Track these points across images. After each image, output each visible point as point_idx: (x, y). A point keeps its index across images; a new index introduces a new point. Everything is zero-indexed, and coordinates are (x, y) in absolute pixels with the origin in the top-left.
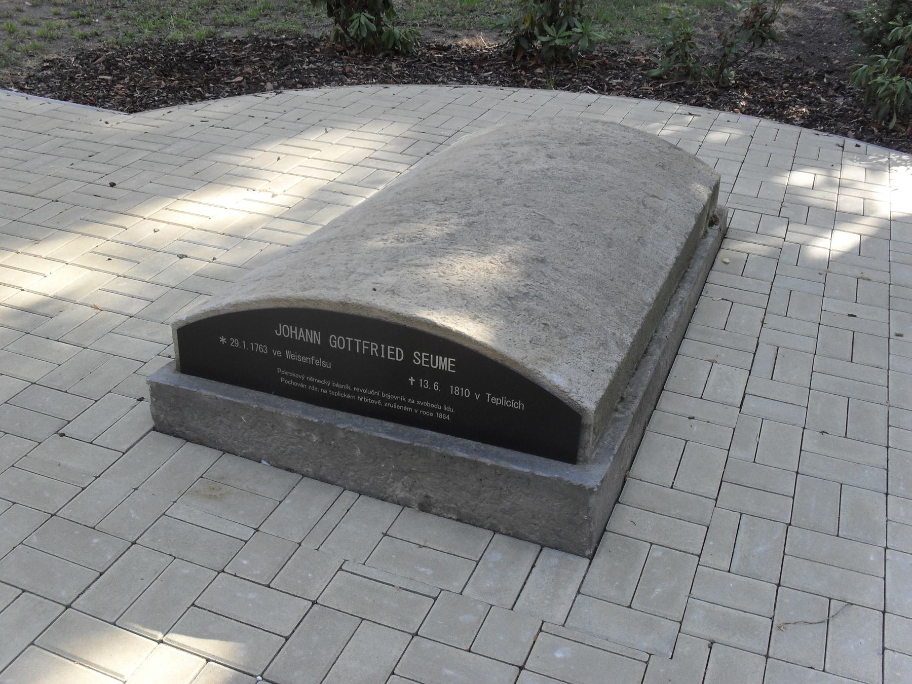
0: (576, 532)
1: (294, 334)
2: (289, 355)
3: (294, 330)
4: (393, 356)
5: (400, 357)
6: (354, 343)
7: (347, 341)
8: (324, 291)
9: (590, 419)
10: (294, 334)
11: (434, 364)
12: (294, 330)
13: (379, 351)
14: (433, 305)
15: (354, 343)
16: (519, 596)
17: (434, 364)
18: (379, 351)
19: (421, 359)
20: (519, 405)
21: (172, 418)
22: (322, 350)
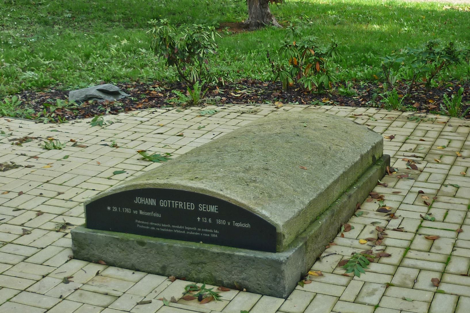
2: (141, 212)
7: (168, 202)
19: (202, 208)
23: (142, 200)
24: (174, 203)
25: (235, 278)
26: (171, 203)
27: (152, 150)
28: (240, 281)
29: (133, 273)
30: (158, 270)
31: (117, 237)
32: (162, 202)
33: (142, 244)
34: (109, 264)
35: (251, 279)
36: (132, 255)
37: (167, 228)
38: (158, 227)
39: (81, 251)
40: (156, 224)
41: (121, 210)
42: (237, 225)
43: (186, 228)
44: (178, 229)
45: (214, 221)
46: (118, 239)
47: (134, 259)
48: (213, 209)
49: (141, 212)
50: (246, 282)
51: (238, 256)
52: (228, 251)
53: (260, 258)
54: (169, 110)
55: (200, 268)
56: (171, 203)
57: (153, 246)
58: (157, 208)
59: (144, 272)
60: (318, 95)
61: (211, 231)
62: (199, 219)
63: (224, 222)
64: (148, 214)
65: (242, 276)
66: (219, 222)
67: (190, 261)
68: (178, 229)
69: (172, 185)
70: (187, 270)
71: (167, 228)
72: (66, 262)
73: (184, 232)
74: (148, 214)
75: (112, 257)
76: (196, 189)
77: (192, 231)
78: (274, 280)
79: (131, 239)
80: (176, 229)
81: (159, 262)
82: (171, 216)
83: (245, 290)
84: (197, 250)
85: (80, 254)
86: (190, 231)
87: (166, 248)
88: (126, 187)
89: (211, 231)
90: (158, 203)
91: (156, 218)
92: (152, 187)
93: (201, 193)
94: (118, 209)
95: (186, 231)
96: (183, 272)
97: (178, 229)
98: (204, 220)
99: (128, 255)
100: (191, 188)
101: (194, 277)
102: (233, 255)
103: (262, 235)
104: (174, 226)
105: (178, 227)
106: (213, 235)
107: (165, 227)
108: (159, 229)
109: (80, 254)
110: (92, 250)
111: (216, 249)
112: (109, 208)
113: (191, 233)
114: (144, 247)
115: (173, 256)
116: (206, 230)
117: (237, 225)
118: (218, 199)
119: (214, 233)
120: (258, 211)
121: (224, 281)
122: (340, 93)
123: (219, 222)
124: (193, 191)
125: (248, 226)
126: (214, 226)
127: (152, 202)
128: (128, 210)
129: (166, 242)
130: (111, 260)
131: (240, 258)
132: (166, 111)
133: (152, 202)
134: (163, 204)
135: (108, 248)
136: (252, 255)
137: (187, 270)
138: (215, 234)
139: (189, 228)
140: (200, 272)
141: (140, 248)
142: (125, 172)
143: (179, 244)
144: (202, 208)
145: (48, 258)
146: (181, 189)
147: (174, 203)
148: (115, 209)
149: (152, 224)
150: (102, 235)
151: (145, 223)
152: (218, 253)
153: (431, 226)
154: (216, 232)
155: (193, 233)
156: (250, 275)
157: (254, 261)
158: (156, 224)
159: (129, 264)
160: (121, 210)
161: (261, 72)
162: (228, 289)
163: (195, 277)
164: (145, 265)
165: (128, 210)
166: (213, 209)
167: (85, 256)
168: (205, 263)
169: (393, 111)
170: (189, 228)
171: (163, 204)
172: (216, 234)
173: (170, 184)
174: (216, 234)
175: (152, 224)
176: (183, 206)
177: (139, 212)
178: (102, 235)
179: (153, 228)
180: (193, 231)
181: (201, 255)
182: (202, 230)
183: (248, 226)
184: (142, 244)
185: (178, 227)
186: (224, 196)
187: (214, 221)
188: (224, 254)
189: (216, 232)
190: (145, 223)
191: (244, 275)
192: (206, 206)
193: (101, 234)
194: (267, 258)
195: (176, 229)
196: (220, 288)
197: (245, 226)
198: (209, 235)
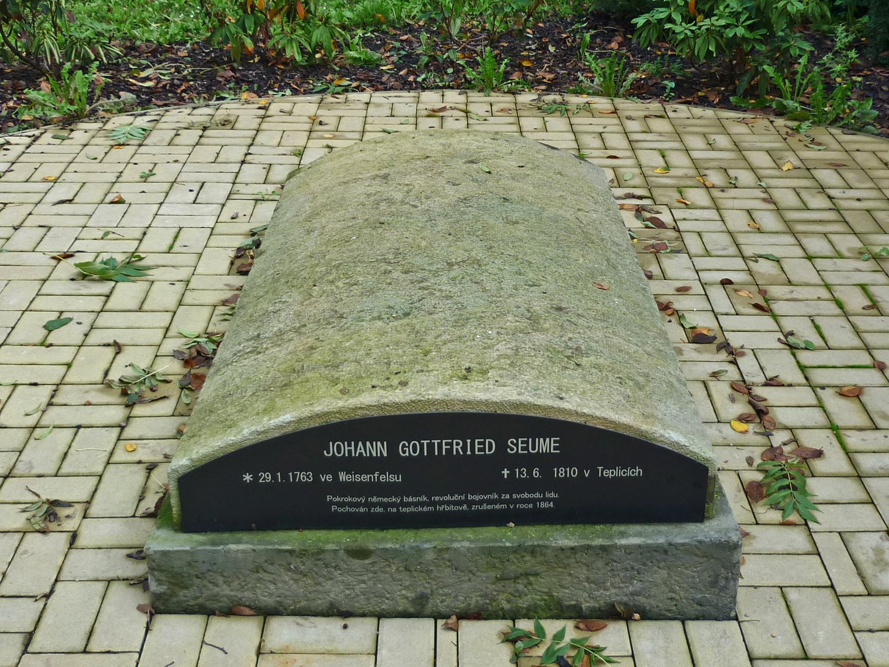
1: (350, 451)
2: (343, 477)
3: (349, 445)
5: (490, 450)
7: (422, 445)
12: (349, 445)
13: (464, 448)
19: (516, 446)
20: (393, 478)
23: (345, 448)
24: (440, 445)
25: (613, 593)
26: (431, 447)
27: (91, 250)
28: (625, 599)
29: (345, 627)
30: (402, 605)
31: (288, 547)
32: (404, 446)
33: (361, 553)
34: (266, 613)
35: (654, 591)
36: (330, 582)
37: (416, 504)
38: (393, 505)
39: (168, 592)
40: (385, 500)
41: (285, 476)
42: (609, 473)
43: (470, 497)
44: (448, 502)
45: (547, 472)
46: (291, 552)
47: (334, 591)
48: (546, 445)
49: (343, 477)
50: (641, 600)
51: (626, 547)
52: (596, 536)
53: (683, 545)
54: (36, 138)
55: (521, 587)
56: (431, 447)
57: (389, 555)
58: (391, 463)
59: (364, 615)
60: (312, 73)
61: (537, 495)
62: (506, 472)
63: (573, 472)
64: (365, 478)
65: (631, 589)
66: (561, 473)
67: (492, 574)
68: (448, 503)
69: (432, 402)
70: (485, 596)
71: (416, 504)
72: (148, 629)
73: (465, 507)
74: (365, 478)
75: (271, 595)
76: (501, 404)
77: (485, 501)
78: (714, 584)
79: (330, 547)
80: (441, 503)
81: (407, 588)
82: (422, 475)
83: (637, 616)
84: (518, 549)
85: (175, 599)
86: (480, 503)
87: (430, 556)
88: (300, 421)
89: (537, 495)
90: (392, 449)
91: (388, 484)
92: (375, 413)
93: (513, 412)
94: (274, 477)
95: (470, 503)
96: (475, 600)
97: (448, 503)
98: (520, 473)
99: (319, 584)
100: (486, 403)
101: (502, 609)
102: (615, 546)
103: (676, 486)
104: (437, 498)
105: (448, 498)
106: (544, 505)
107: (415, 503)
108: (395, 510)
109: (175, 599)
110: (211, 586)
111: (564, 537)
112: (248, 478)
113: (485, 507)
114: (367, 561)
115: (448, 571)
116: (526, 495)
117: (609, 473)
118: (659, 447)
119: (545, 499)
120: (662, 436)
121: (583, 606)
122: (350, 61)
123: (561, 473)
124: (491, 410)
125: (638, 471)
126: (547, 483)
127: (379, 449)
128: (303, 477)
129: (429, 540)
130: (268, 601)
131: (629, 550)
132: (29, 140)
133: (379, 449)
134: (407, 449)
135: (262, 575)
136: (661, 540)
137: (485, 596)
138: (547, 501)
139: (477, 498)
140: (521, 595)
141: (356, 563)
142: (71, 319)
143: (464, 540)
144: (516, 446)
145: (88, 629)
146: (457, 409)
147: (440, 445)
148: (266, 477)
149: (375, 499)
150: (242, 547)
151: (355, 499)
152: (572, 549)
153: (856, 364)
154: (552, 495)
155: (489, 507)
156: (656, 584)
157: (666, 552)
158: (385, 500)
159: (321, 603)
160: (285, 476)
161: (146, 25)
162: (601, 622)
163: (506, 606)
164: (368, 599)
165: (303, 477)
166: (546, 445)
167: (192, 603)
168: (536, 575)
169: (492, 94)
170: (477, 498)
171: (407, 449)
172: (549, 500)
173: (428, 401)
174: (549, 500)
175: (375, 499)
176: (464, 448)
177: (336, 477)
178: (242, 547)
179: (379, 510)
180: (490, 502)
181: (527, 558)
182: (514, 496)
183: (638, 471)
184: (361, 553)
185: (448, 498)
186: (569, 412)
187: (547, 472)
188: (589, 547)
189: (552, 495)
190: (355, 499)
191: (637, 585)
192: (527, 442)
193: (241, 545)
194: (700, 542)
195: (441, 503)
196: (581, 626)
197: (629, 473)
198: (531, 506)
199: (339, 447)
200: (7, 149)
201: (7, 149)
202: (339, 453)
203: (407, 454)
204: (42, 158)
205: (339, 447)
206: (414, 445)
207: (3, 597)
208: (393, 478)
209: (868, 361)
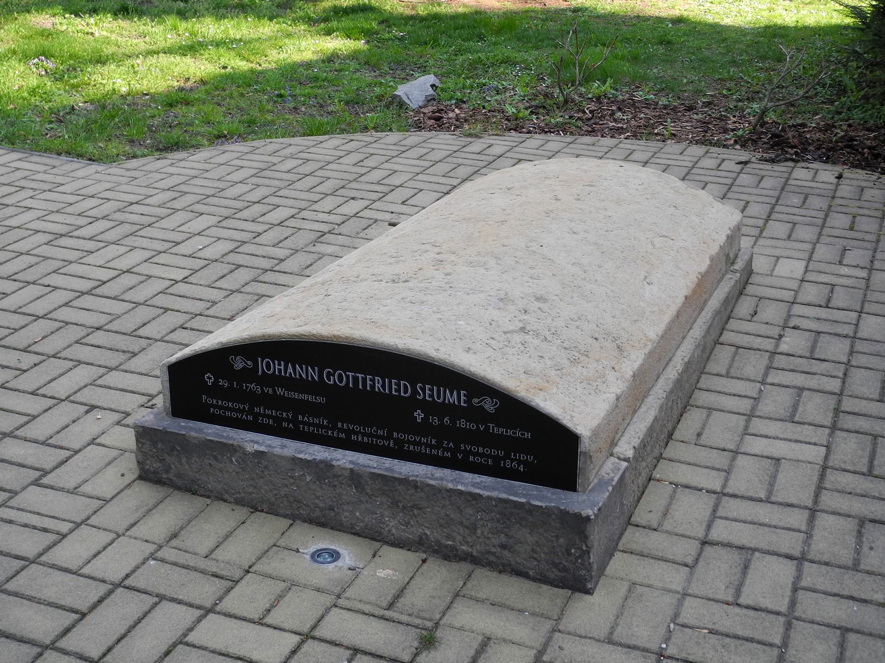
0: (567, 565)
1: (280, 370)
2: (280, 391)
3: (280, 365)
4: (398, 390)
5: (406, 392)
6: (356, 379)
7: (347, 377)
8: (319, 326)
9: (585, 445)
10: (280, 370)
11: (439, 398)
12: (280, 365)
13: (383, 386)
14: (210, 313)
15: (356, 379)
16: (118, 493)
17: (439, 398)
18: (383, 386)
19: (427, 392)
20: (320, 400)
21: (160, 463)
22: (318, 387)
147: (364, 380)
199: (268, 364)
200: (556, 565)
201: (556, 565)
202: (405, 385)
203: (332, 382)
204: (460, 161)
205: (268, 364)
206: (340, 375)
207: (3, 461)
208: (320, 400)
209: (140, 603)
